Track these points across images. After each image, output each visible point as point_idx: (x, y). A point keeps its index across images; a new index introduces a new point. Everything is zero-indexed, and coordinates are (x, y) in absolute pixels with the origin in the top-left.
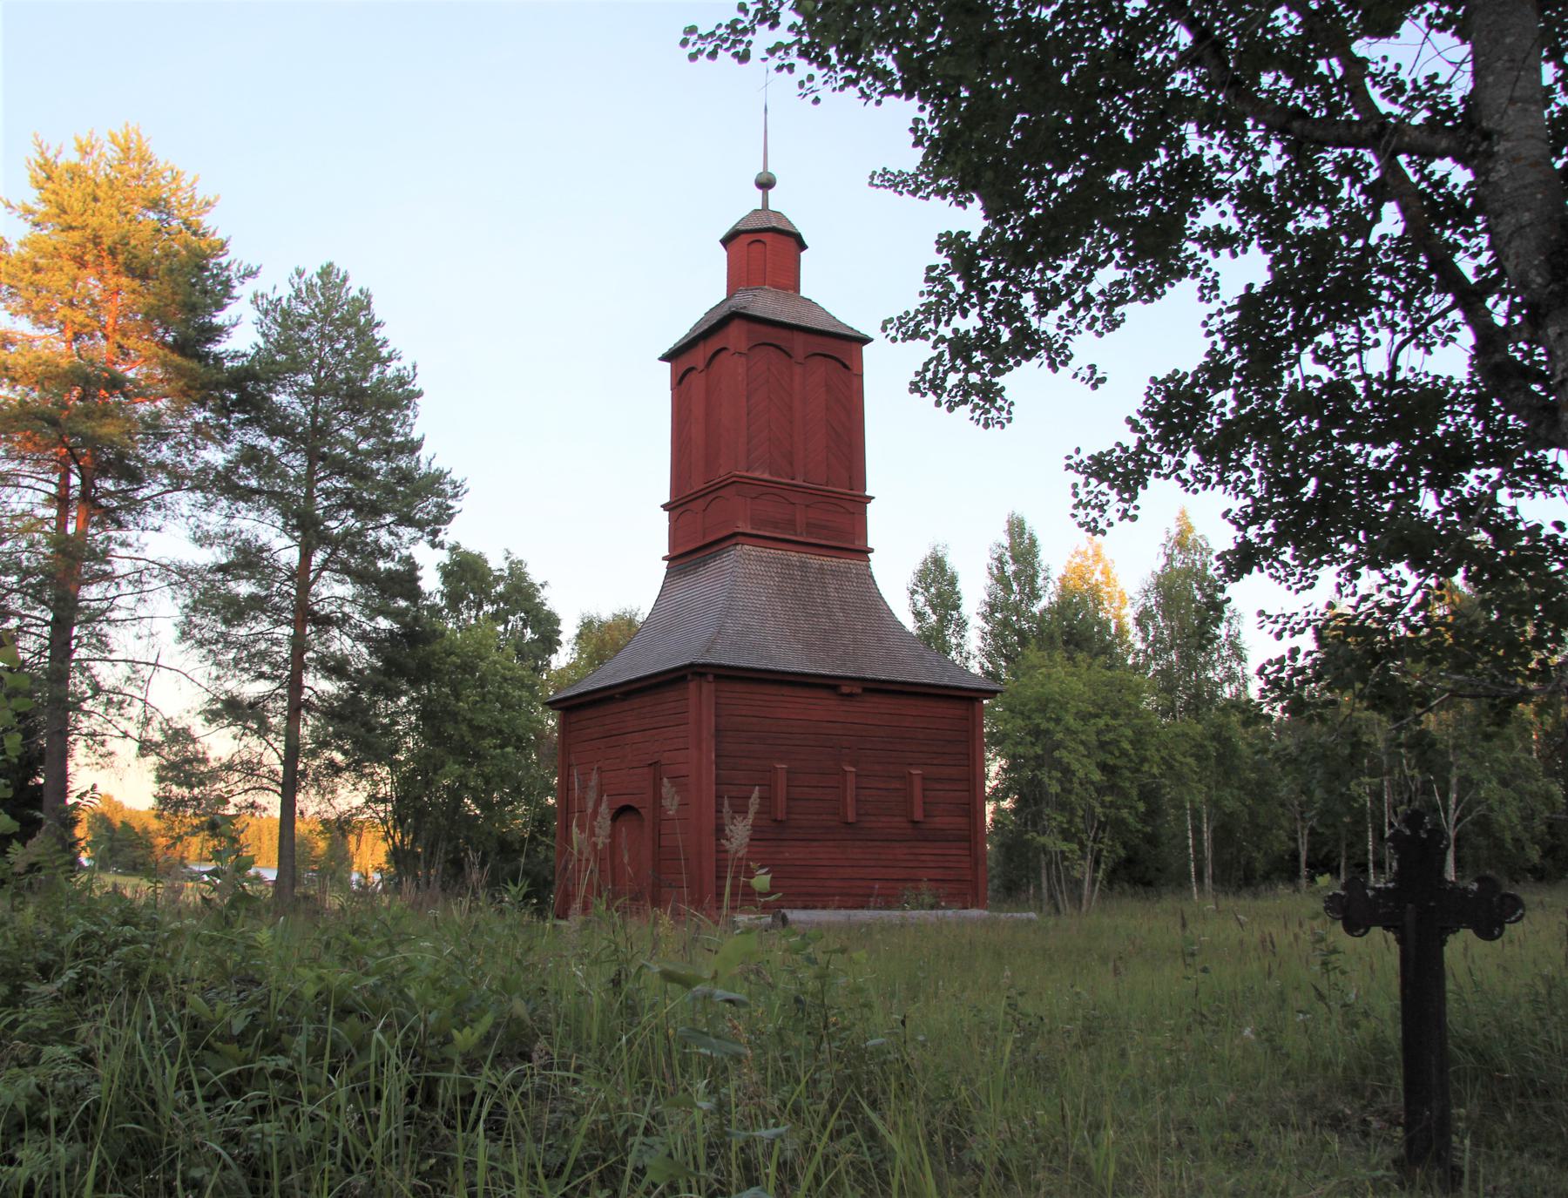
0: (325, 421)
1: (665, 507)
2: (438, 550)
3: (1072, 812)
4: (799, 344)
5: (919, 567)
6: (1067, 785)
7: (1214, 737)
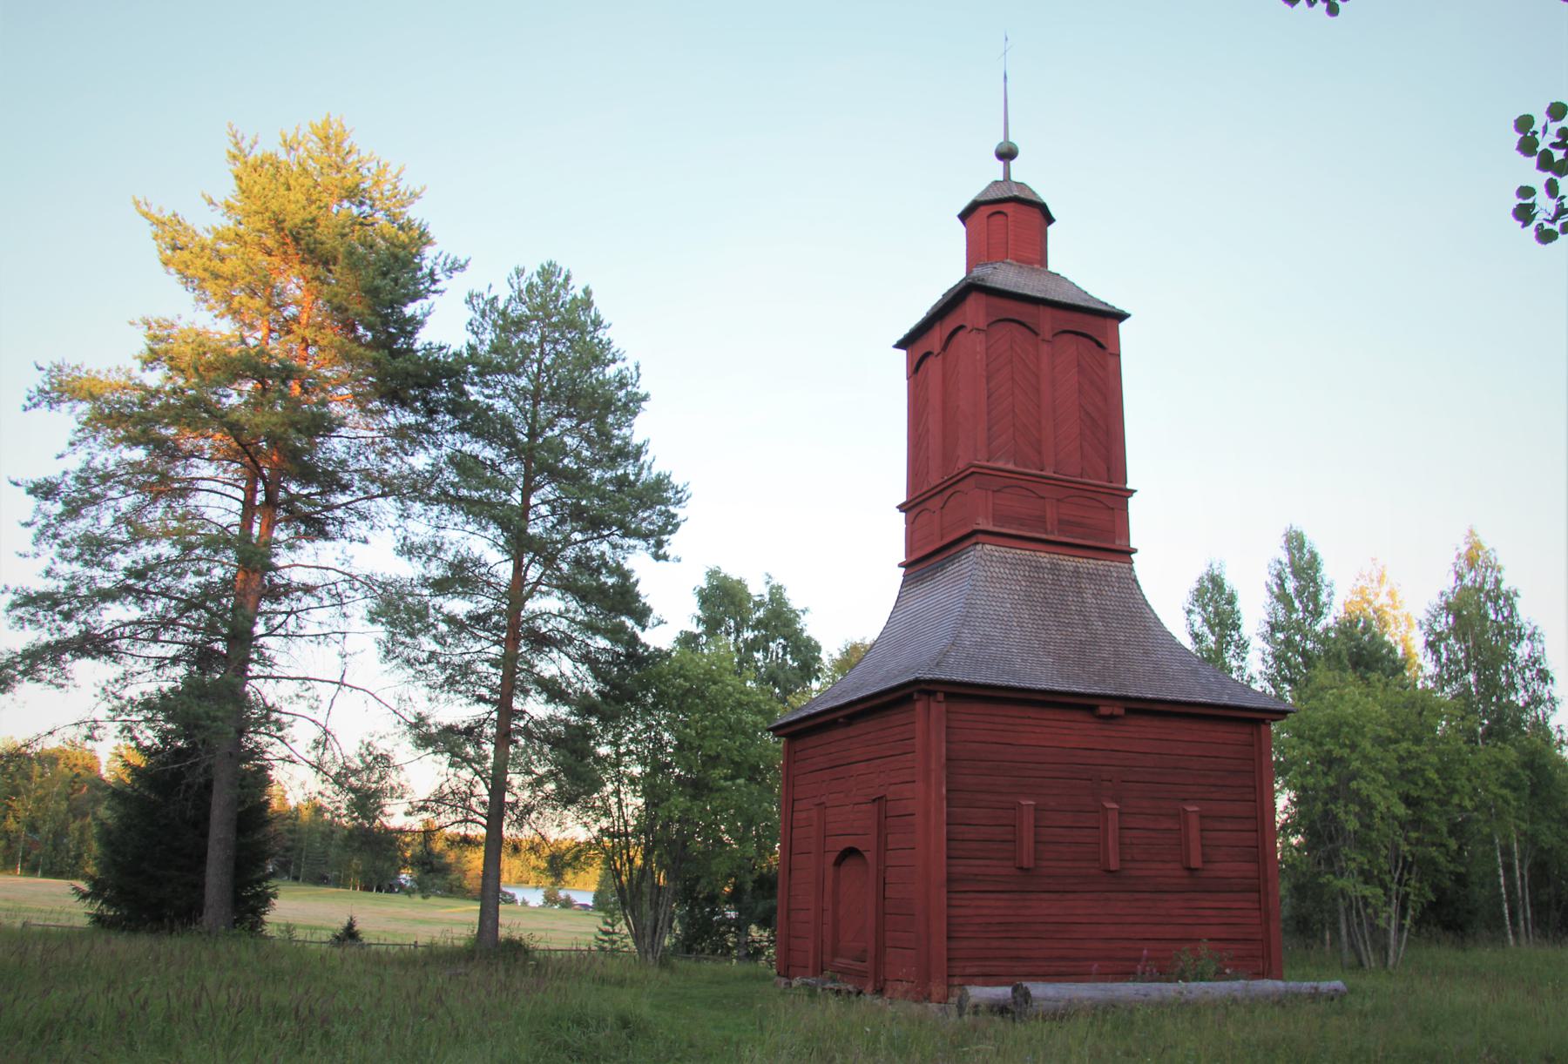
0: (551, 434)
1: (901, 508)
2: (662, 562)
3: (1376, 853)
4: (1047, 321)
5: (1196, 586)
6: (1367, 820)
7: (1525, 765)
